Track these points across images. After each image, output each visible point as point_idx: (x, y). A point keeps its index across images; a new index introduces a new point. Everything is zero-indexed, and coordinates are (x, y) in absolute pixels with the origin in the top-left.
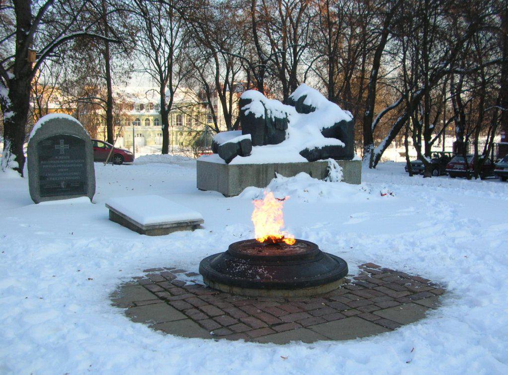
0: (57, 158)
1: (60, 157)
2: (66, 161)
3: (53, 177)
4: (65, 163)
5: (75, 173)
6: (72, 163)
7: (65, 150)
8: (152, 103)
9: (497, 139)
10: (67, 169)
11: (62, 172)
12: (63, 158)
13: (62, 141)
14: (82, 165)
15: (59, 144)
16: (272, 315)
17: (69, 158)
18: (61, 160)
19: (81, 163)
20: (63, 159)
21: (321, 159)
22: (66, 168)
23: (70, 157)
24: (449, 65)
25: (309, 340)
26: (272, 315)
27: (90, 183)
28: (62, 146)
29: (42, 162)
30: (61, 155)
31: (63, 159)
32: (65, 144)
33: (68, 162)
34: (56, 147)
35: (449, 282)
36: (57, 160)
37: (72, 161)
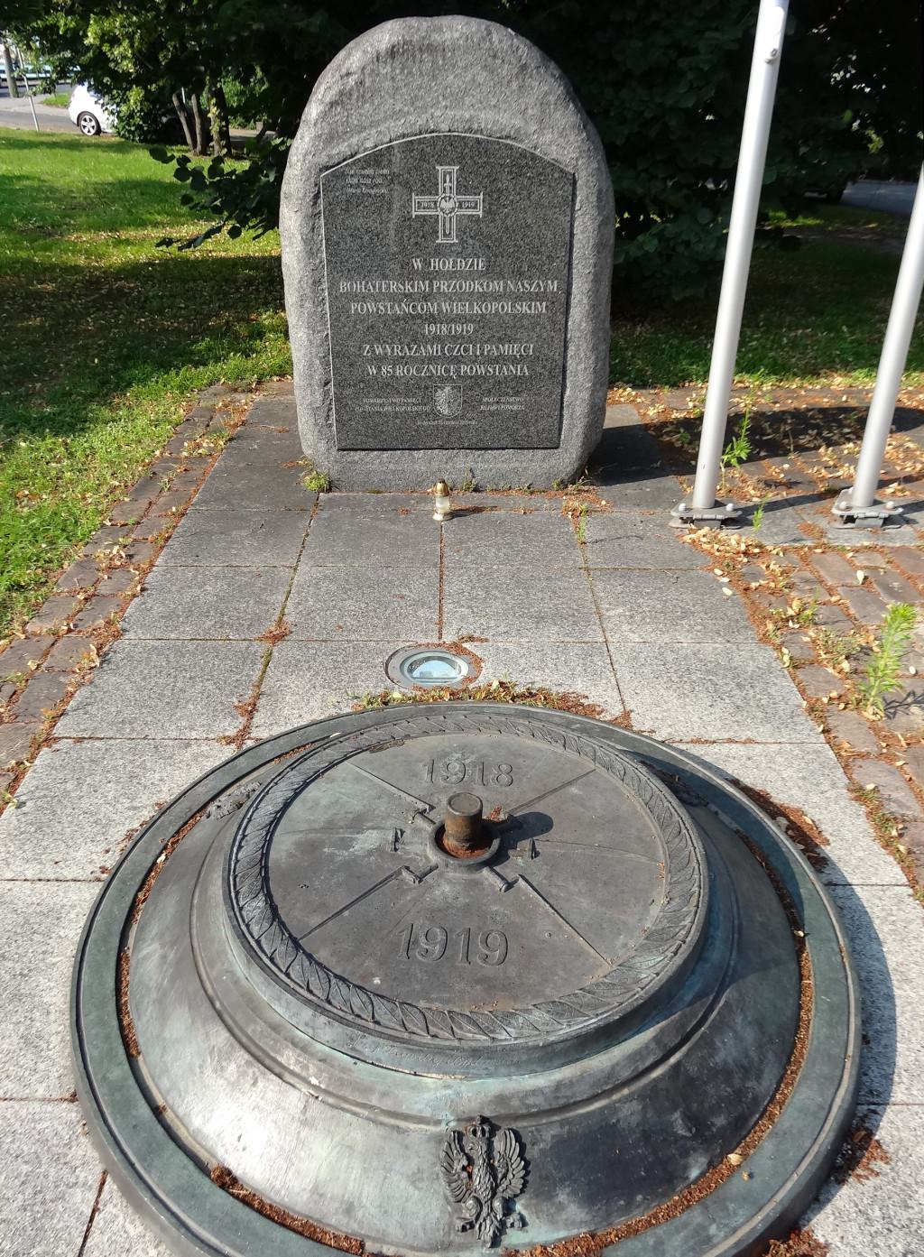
1: (436, 264)
2: (466, 286)
4: (460, 297)
5: (506, 349)
8: (229, 1173)
10: (471, 327)
11: (437, 339)
12: (449, 266)
13: (447, 173)
14: (542, 307)
15: (430, 187)
16: (186, 823)
21: (499, 847)
22: (461, 319)
23: (488, 266)
25: (871, 922)
26: (186, 823)
27: (605, 290)
28: (449, 205)
29: (344, 286)
30: (440, 252)
31: (452, 275)
34: (419, 206)
37: (497, 286)
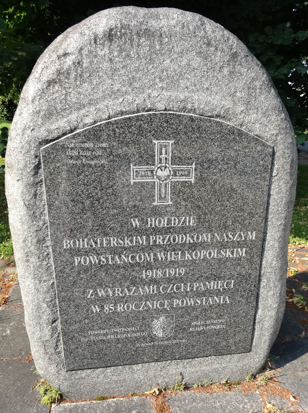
0: (136, 223)
3: (117, 301)
4: (174, 248)
6: (203, 246)
7: (179, 190)
9: (301, 55)
10: (183, 271)
11: (154, 281)
17: (192, 222)
18: (156, 231)
19: (240, 245)
20: (168, 230)
24: (13, 8)
30: (156, 212)
31: (168, 230)
32: (176, 160)
33: (189, 239)
35: (274, 109)
36: (139, 232)
37: (206, 237)
